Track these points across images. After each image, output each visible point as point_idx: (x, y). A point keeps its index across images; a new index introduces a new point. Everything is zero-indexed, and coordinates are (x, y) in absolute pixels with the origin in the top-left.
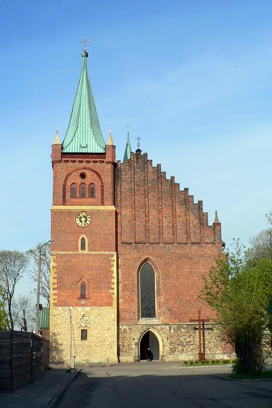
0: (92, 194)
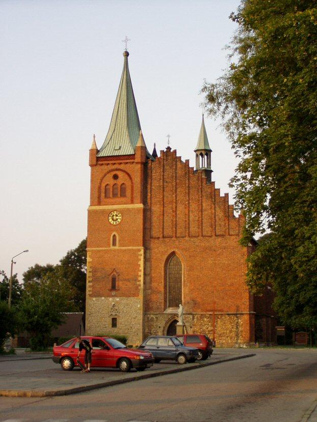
0: (123, 194)
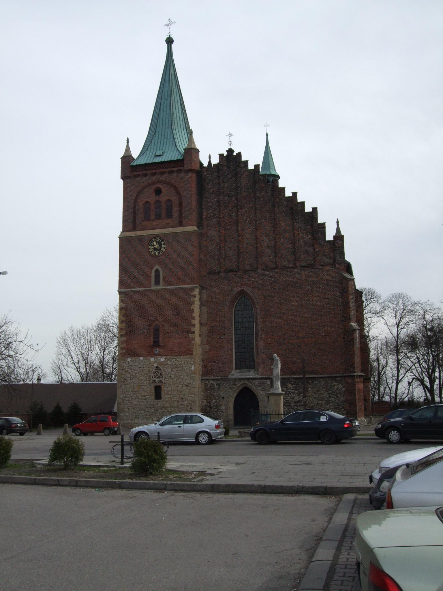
0: (169, 215)
